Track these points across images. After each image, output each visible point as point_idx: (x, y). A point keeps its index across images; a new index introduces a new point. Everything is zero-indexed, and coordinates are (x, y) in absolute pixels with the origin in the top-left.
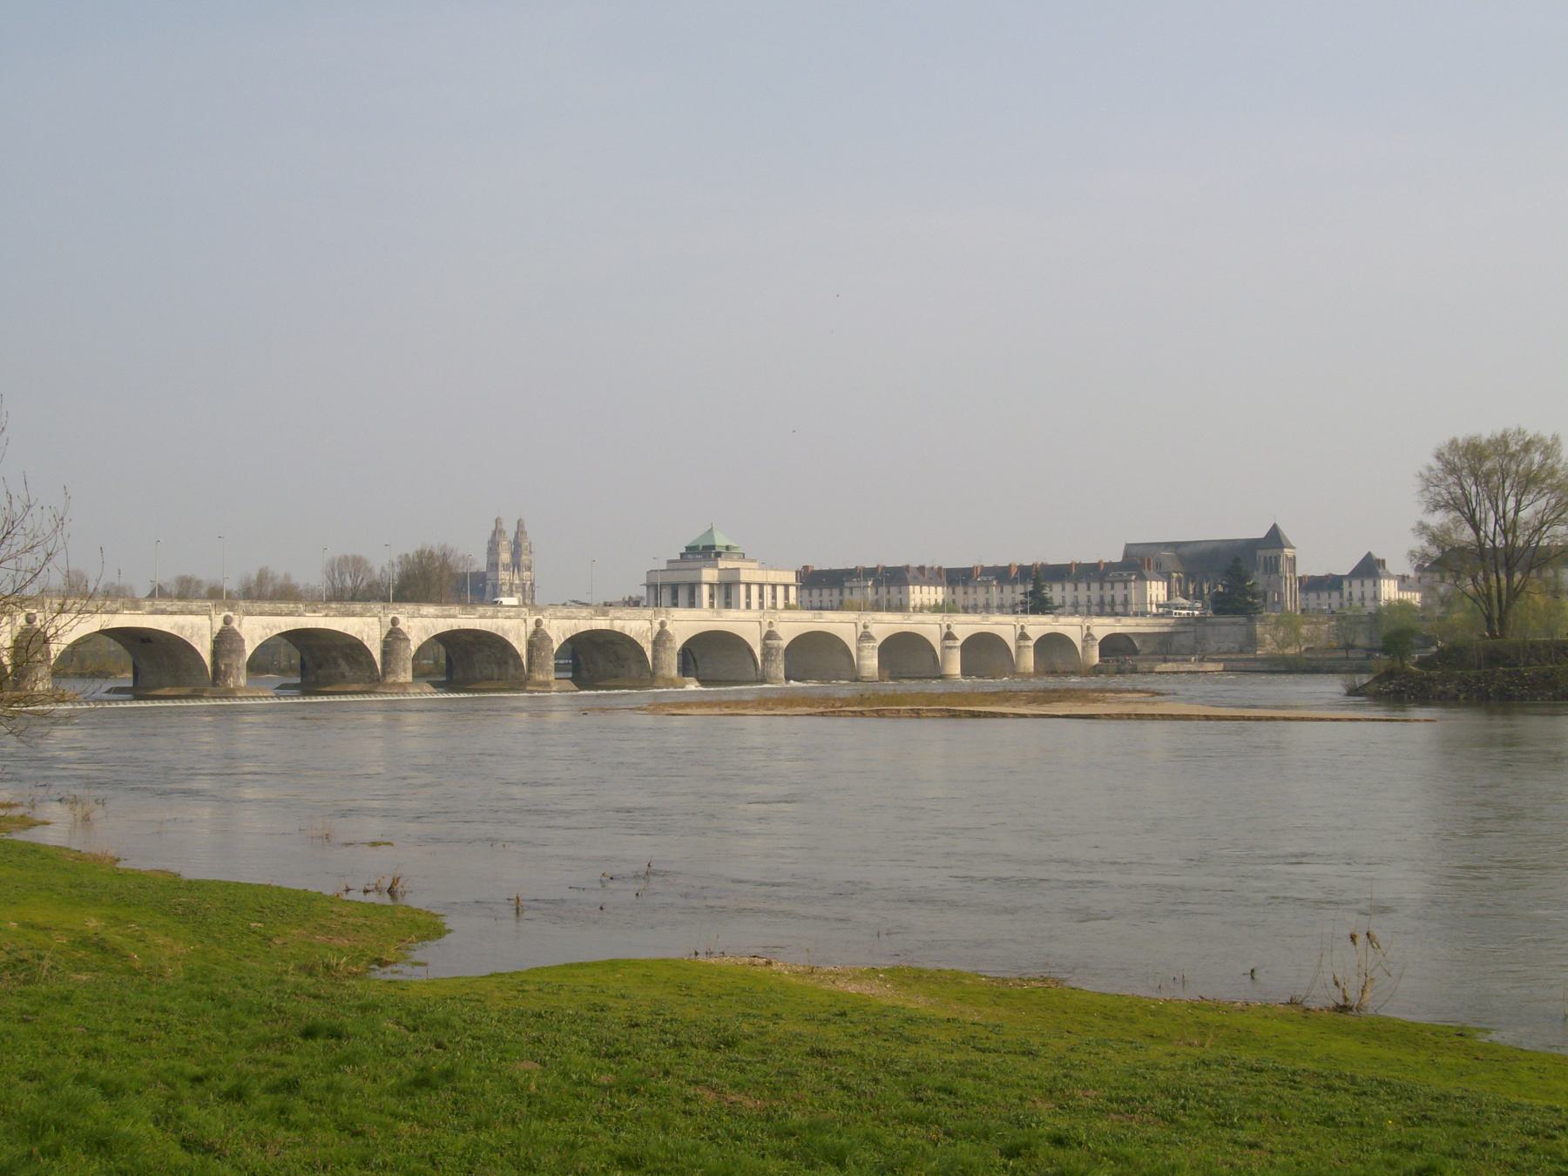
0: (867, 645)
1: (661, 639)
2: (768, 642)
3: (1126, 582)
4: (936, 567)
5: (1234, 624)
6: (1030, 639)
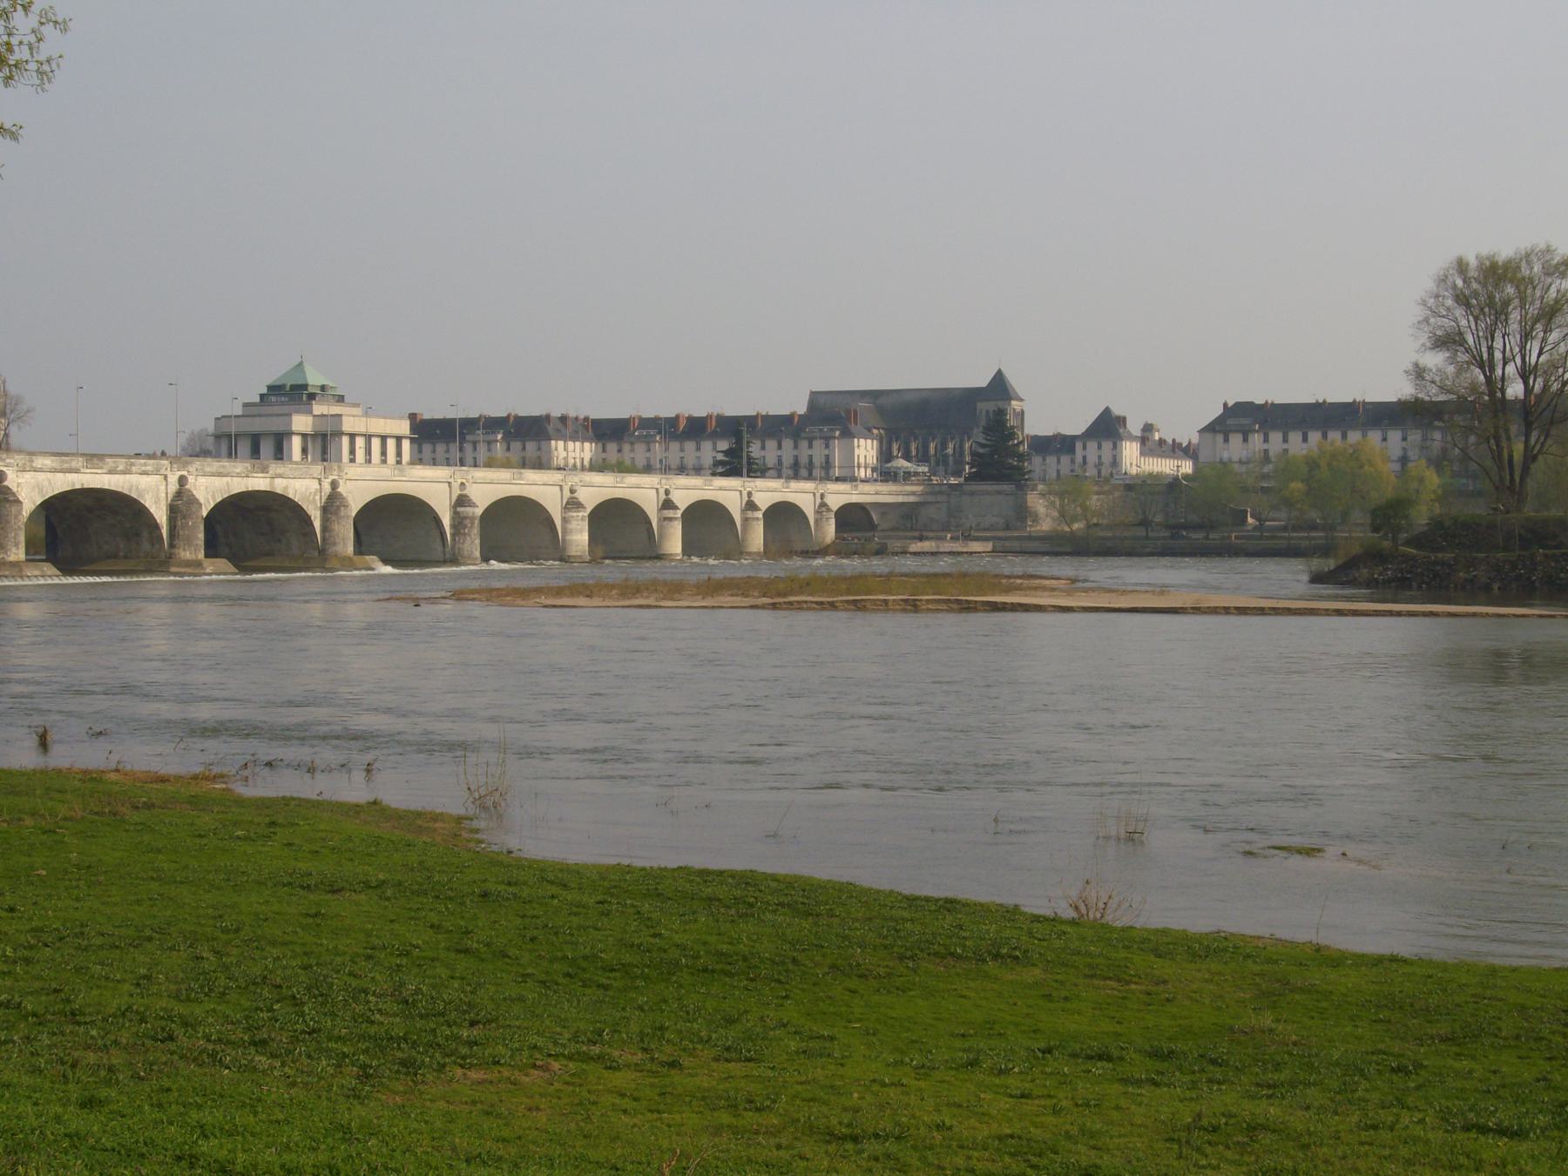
0: (575, 514)
1: (333, 504)
2: (459, 509)
3: (827, 440)
4: (582, 417)
5: (999, 493)
6: (760, 510)
